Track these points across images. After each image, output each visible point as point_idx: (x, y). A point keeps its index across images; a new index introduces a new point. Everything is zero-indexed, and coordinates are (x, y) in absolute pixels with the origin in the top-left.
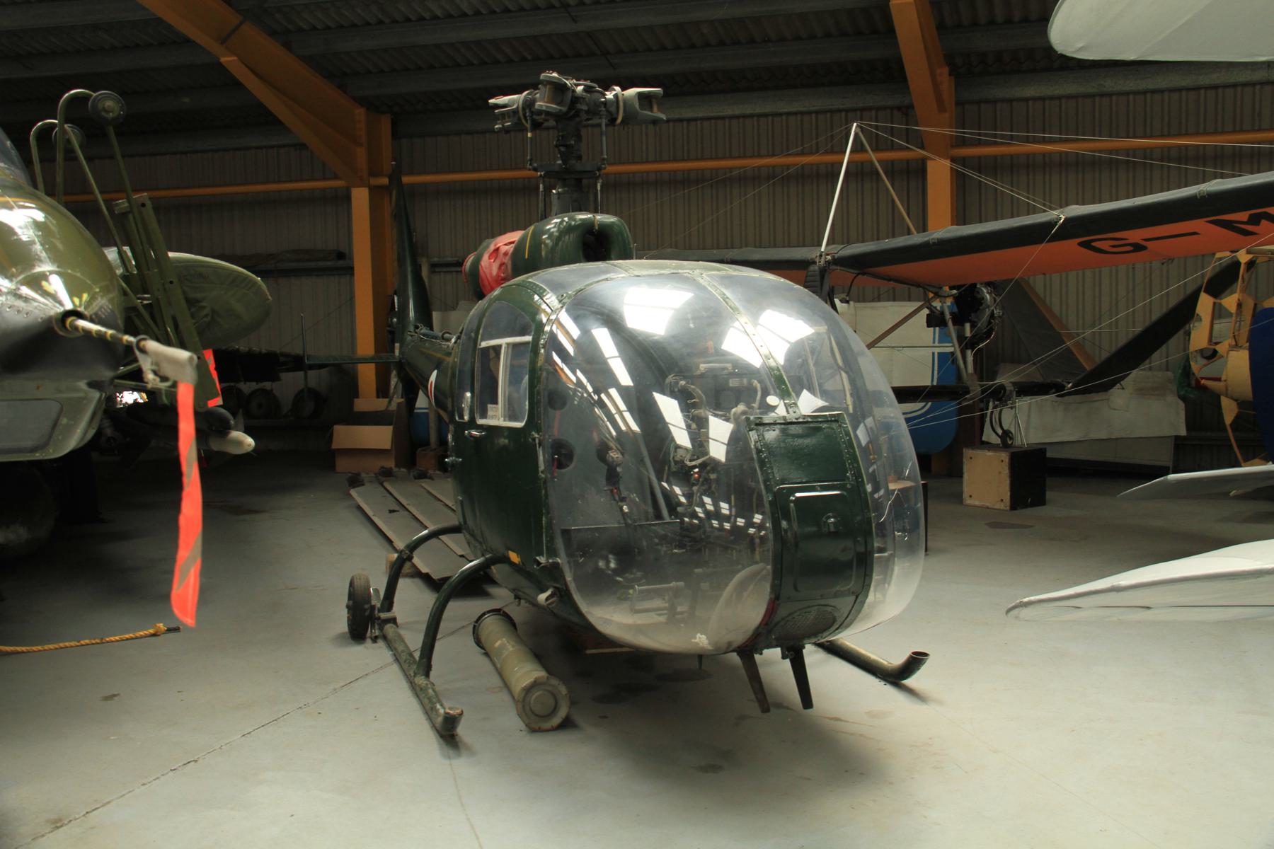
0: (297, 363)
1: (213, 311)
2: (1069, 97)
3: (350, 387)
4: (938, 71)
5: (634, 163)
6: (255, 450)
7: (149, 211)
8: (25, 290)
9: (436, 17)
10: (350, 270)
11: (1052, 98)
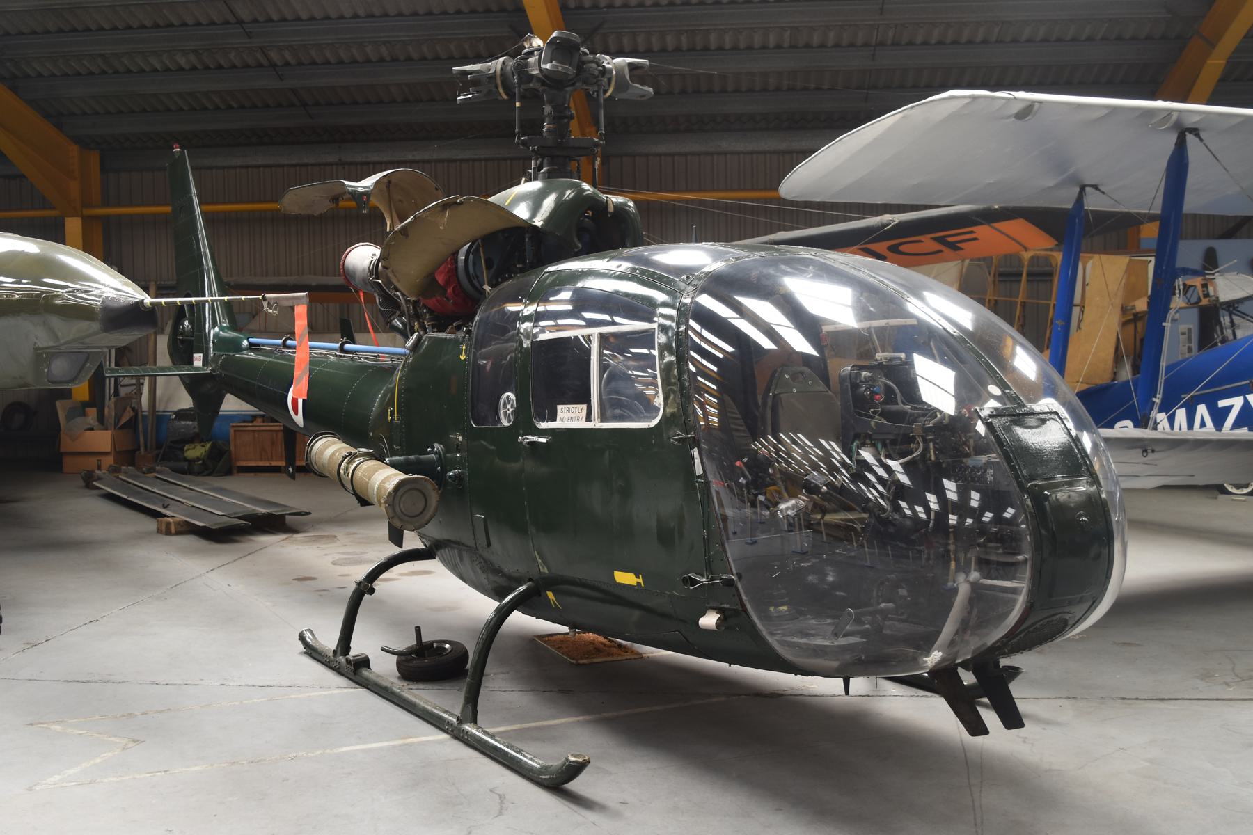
2: (693, 154)
4: (587, 130)
5: (265, 202)
9: (156, 70)
11: (680, 154)
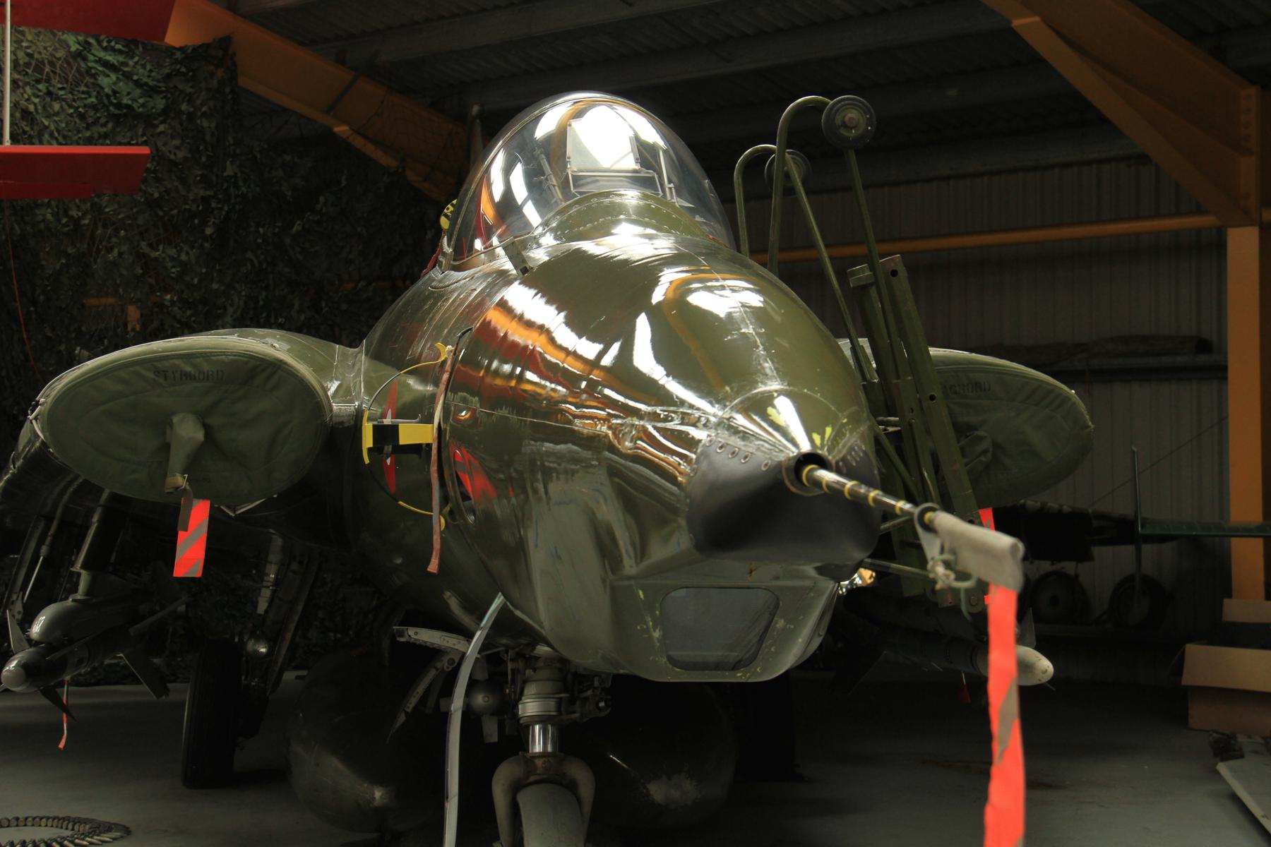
0: (1123, 530)
1: (997, 446)
3: (1220, 580)
6: (1053, 680)
7: (903, 282)
8: (740, 420)
10: (1219, 372)
